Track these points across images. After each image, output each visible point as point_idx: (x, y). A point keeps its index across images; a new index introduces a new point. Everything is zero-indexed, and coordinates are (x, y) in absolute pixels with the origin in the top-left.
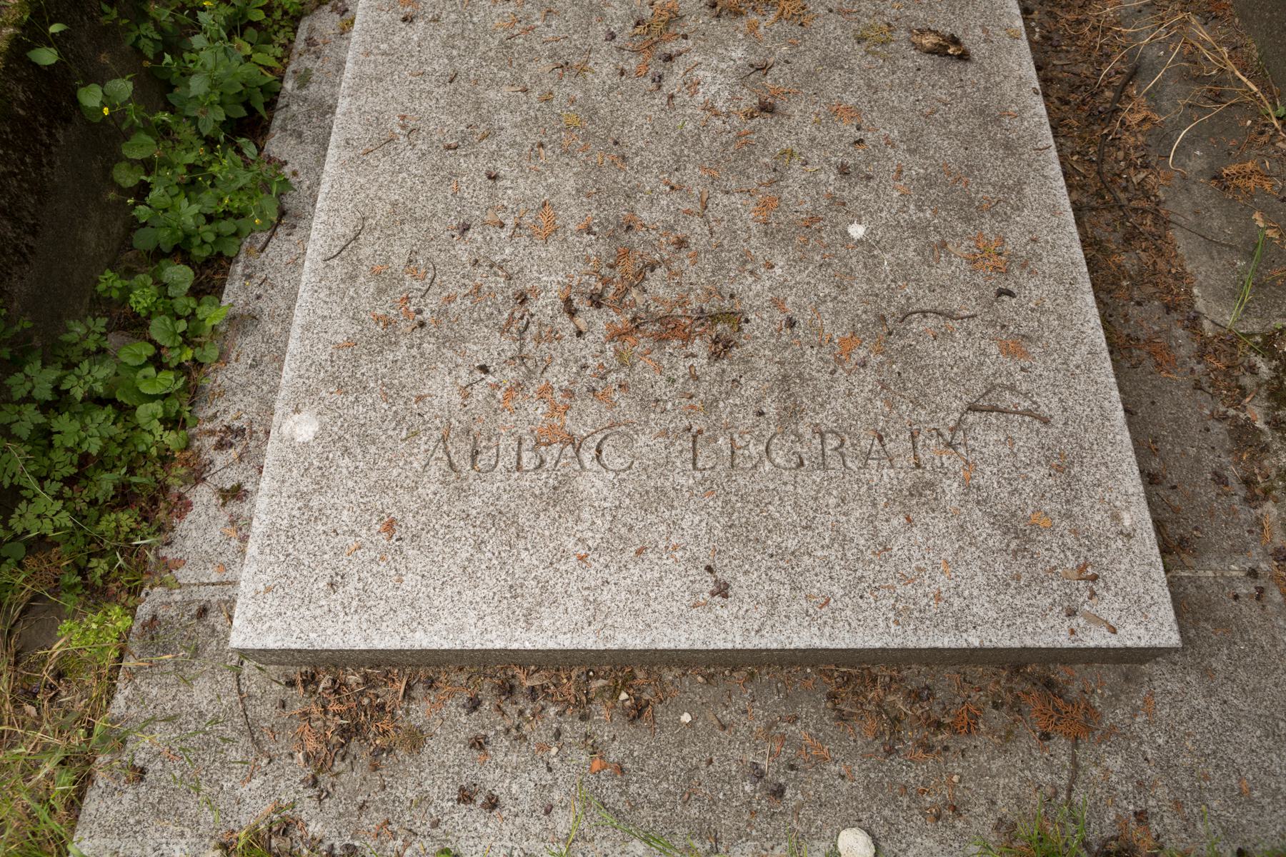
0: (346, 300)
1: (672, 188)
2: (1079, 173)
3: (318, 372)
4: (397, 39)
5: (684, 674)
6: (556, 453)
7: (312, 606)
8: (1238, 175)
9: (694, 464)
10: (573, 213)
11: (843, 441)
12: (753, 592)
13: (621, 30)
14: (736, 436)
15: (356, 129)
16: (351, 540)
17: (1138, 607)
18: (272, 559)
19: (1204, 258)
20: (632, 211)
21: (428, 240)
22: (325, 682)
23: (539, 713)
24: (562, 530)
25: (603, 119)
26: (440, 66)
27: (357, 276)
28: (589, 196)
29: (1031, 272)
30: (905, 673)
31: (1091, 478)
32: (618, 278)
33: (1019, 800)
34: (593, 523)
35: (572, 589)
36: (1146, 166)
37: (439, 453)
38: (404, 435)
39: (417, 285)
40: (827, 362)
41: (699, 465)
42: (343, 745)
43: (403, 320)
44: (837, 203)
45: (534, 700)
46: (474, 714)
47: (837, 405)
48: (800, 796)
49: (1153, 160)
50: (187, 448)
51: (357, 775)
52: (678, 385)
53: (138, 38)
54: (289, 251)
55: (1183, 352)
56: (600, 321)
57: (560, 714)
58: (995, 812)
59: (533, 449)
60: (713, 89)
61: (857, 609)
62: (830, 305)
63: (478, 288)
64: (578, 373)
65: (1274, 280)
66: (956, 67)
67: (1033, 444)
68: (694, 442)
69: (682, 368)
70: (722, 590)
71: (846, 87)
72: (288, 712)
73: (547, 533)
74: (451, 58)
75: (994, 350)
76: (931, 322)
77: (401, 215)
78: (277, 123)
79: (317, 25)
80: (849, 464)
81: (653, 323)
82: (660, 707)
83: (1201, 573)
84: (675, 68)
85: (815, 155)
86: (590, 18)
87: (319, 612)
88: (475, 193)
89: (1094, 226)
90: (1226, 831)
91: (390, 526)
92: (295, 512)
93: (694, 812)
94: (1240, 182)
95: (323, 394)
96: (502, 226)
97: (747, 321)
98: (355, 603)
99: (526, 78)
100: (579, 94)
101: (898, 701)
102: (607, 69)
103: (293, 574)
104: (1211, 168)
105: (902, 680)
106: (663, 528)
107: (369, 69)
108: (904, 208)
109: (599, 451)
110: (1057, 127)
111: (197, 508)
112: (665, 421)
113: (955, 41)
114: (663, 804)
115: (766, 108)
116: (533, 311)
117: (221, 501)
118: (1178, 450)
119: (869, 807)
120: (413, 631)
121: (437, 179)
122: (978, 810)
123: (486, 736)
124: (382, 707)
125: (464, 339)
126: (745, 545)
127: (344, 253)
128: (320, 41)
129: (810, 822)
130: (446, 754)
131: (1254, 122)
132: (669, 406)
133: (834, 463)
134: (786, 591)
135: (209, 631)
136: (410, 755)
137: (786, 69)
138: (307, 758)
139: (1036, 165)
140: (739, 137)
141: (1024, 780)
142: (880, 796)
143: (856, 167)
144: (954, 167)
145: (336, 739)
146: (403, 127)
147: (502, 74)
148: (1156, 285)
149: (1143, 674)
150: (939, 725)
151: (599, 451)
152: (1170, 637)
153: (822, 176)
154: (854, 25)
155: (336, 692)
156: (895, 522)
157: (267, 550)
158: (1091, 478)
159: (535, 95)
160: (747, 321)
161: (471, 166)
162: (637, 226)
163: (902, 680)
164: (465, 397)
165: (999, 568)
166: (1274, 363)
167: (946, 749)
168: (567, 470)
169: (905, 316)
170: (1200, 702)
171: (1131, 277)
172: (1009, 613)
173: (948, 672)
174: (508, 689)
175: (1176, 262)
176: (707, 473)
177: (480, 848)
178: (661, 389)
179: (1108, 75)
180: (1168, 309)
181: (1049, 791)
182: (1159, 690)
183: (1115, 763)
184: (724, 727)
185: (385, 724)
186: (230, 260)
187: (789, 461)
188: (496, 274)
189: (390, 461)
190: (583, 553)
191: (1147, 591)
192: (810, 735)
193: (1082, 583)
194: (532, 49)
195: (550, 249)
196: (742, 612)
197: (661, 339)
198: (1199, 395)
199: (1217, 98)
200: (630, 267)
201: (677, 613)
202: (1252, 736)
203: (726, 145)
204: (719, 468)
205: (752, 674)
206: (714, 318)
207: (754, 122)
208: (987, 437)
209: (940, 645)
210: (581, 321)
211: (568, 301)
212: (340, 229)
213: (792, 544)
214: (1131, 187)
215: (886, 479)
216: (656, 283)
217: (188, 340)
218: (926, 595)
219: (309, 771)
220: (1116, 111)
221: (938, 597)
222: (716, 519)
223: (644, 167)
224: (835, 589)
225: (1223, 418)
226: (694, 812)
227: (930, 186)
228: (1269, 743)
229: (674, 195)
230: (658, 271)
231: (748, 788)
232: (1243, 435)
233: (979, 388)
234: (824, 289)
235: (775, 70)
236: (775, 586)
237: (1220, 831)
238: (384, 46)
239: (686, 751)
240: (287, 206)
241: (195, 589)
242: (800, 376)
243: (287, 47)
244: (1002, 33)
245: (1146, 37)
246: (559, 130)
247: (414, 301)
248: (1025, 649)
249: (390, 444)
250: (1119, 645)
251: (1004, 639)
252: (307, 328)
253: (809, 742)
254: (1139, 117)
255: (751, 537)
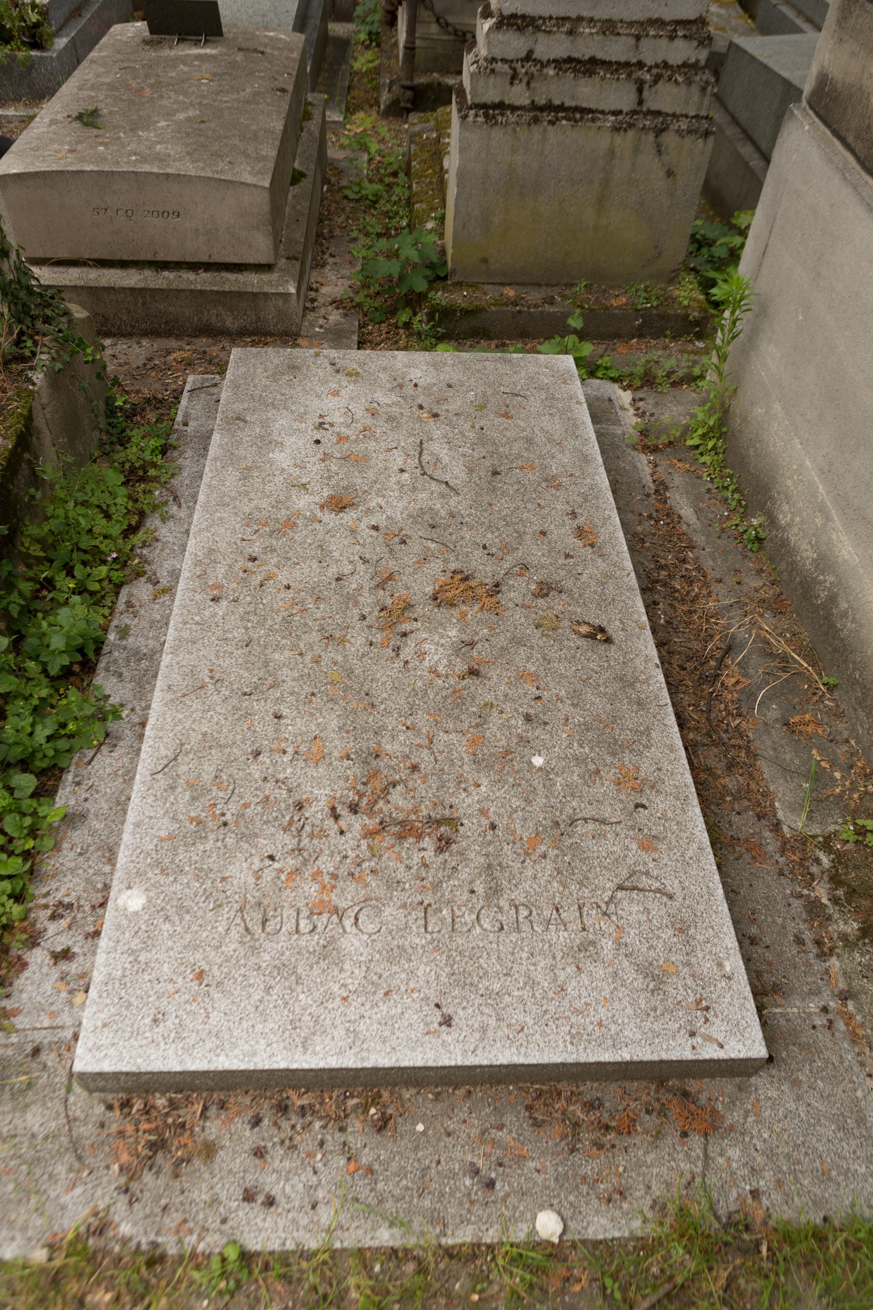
0: (168, 805)
1: (408, 728)
2: (694, 720)
3: (145, 858)
4: (206, 613)
5: (418, 1093)
6: (325, 920)
7: (139, 1038)
8: (801, 723)
9: (426, 929)
10: (336, 745)
11: (531, 912)
12: (470, 1023)
13: (370, 613)
14: (455, 908)
15: (176, 678)
16: (170, 987)
17: (737, 1029)
18: (108, 1001)
19: (782, 781)
20: (379, 744)
21: (229, 763)
22: (138, 1105)
23: (307, 1127)
24: (329, 978)
25: (358, 677)
26: (238, 634)
27: (176, 787)
28: (347, 732)
29: (657, 791)
30: (582, 1088)
31: (702, 937)
32: (369, 792)
33: (668, 1185)
34: (353, 973)
35: (338, 1022)
36: (739, 715)
37: (238, 920)
38: (211, 906)
39: (221, 794)
40: (519, 855)
41: (429, 929)
42: (150, 1158)
43: (212, 821)
44: (524, 741)
45: (303, 1116)
46: (256, 1129)
47: (526, 885)
48: (507, 1188)
49: (744, 710)
50: (24, 919)
51: (161, 1181)
52: (413, 871)
53: (9, 603)
54: (111, 765)
55: (770, 848)
56: (356, 824)
57: (324, 1127)
58: (651, 1195)
59: (308, 918)
60: (436, 658)
61: (544, 1034)
62: (520, 814)
63: (267, 798)
64: (341, 862)
65: (828, 797)
66: (603, 647)
67: (663, 912)
68: (425, 913)
69: (416, 858)
70: (447, 1021)
71: (528, 659)
72: (106, 1132)
73: (319, 980)
74: (246, 629)
75: (634, 846)
76: (591, 826)
77: (209, 742)
78: (102, 665)
79: (135, 592)
80: (536, 928)
81: (396, 825)
82: (400, 1120)
83: (789, 1010)
84: (409, 642)
85: (508, 707)
86: (347, 603)
87: (144, 1042)
88: (264, 728)
89: (705, 758)
90: (815, 1203)
91: (200, 976)
92: (127, 965)
93: (427, 1203)
94: (801, 728)
95: (150, 875)
96: (285, 752)
97: (462, 825)
98: (173, 1035)
99: (302, 645)
100: (340, 658)
101: (577, 1110)
102: (360, 641)
103: (125, 1013)
104: (783, 717)
105: (579, 1094)
106: (403, 976)
107: (186, 635)
108: (570, 746)
109: (356, 919)
110: (673, 687)
111: (31, 968)
112: (404, 897)
113: (602, 630)
114: (403, 1198)
115: (473, 673)
116: (307, 815)
117: (53, 961)
118: (769, 919)
119: (559, 1194)
120: (218, 1056)
121: (236, 716)
122: (638, 1194)
123: (265, 1147)
124: (183, 1125)
125: (256, 836)
126: (463, 988)
127: (166, 770)
128: (137, 604)
129: (515, 1208)
130: (233, 1162)
131: (810, 686)
132: (407, 886)
133: (525, 927)
134: (493, 1022)
135: (41, 1066)
136: (205, 1164)
137: (487, 645)
138: (121, 1169)
139: (659, 717)
140: (454, 692)
141: (671, 1169)
142: (567, 1185)
143: (536, 715)
144: (604, 717)
145: (146, 1152)
146: (212, 678)
147: (284, 641)
148: (750, 800)
149: (750, 1085)
150: (607, 1128)
151: (356, 919)
152: (760, 1051)
153: (513, 722)
154: (533, 615)
155: (147, 1113)
156: (569, 970)
157: (105, 995)
158: (702, 937)
159: (308, 658)
160: (462, 825)
161: (262, 708)
162: (383, 755)
163: (579, 1094)
164: (258, 879)
165: (642, 1003)
166: (832, 856)
167: (613, 1146)
168: (333, 933)
169: (573, 822)
170: (791, 1106)
171: (732, 795)
172: (650, 1035)
173: (613, 1087)
174: (283, 1108)
175: (762, 784)
176: (435, 935)
177: (260, 1239)
178: (401, 873)
179: (711, 650)
180: (760, 817)
181: (688, 1176)
182: (762, 1097)
183: (735, 1153)
184: (449, 1135)
185: (184, 1139)
186: (62, 770)
187: (493, 926)
188: (280, 788)
189: (201, 926)
190: (345, 995)
191: (743, 1018)
192: (514, 1139)
193: (699, 1012)
194: (306, 624)
195: (320, 770)
196: (461, 1038)
197: (401, 837)
198: (783, 880)
199: (784, 670)
200: (378, 784)
201: (414, 1039)
202: (828, 1130)
203: (445, 698)
204: (443, 932)
205: (469, 1092)
206: (439, 822)
207: (465, 682)
208: (631, 908)
209: (602, 1059)
210: (342, 823)
211: (333, 809)
212: (163, 752)
213: (496, 987)
214: (730, 730)
215: (561, 939)
216: (396, 796)
217: (33, 832)
218: (592, 1023)
219: (123, 1180)
220: (718, 676)
221: (600, 1024)
222: (442, 969)
223: (388, 713)
224: (528, 1019)
225: (800, 896)
226: (427, 1203)
227: (588, 730)
228: (840, 1134)
229: (409, 733)
230: (398, 788)
231: (468, 1182)
232: (814, 908)
233: (625, 873)
234: (516, 803)
235: (479, 646)
236: (485, 1018)
237: (810, 1203)
238: (197, 618)
239: (420, 1154)
240: (109, 730)
241: (29, 1032)
242: (500, 864)
243: (112, 609)
244: (634, 625)
245: (736, 626)
246: (326, 684)
247: (219, 806)
248: (662, 1062)
249: (200, 914)
250: (726, 1057)
251: (646, 1054)
252: (137, 825)
253: (512, 1143)
254: (733, 680)
255: (468, 982)
